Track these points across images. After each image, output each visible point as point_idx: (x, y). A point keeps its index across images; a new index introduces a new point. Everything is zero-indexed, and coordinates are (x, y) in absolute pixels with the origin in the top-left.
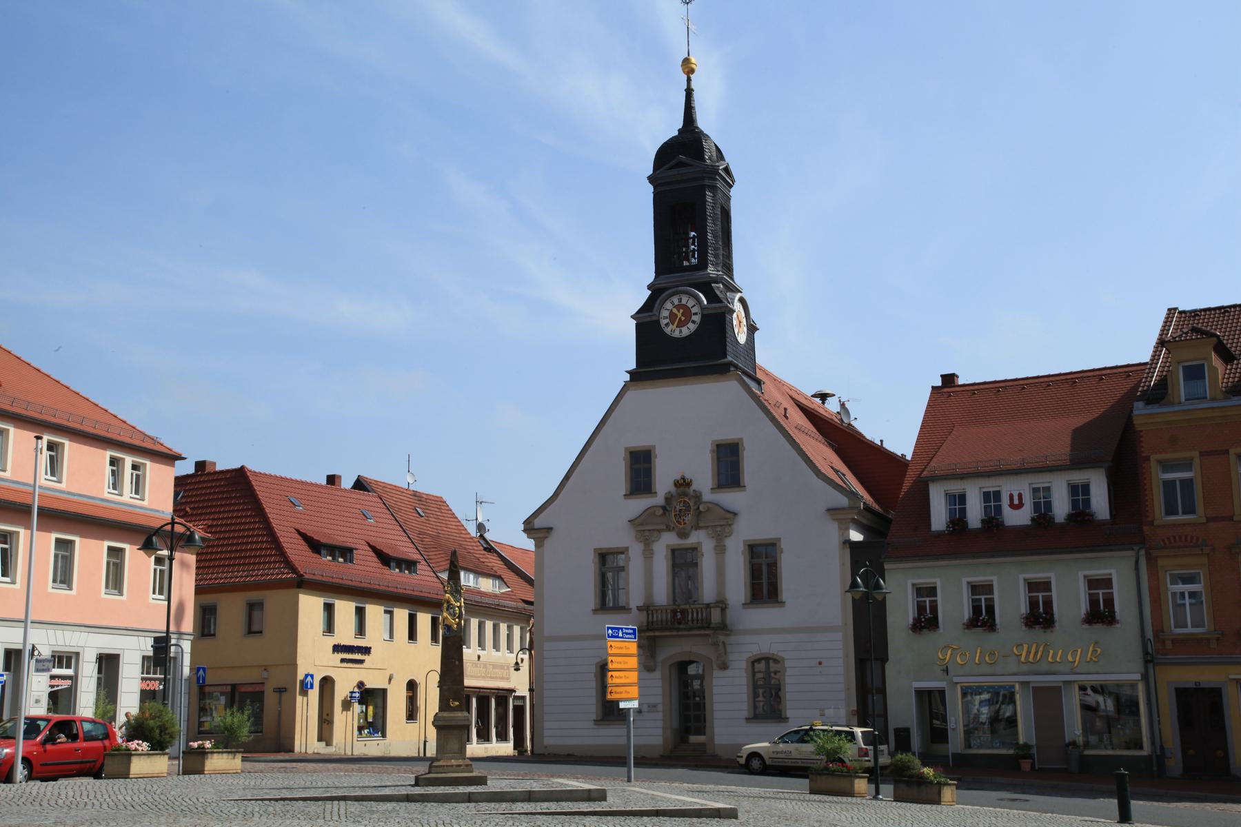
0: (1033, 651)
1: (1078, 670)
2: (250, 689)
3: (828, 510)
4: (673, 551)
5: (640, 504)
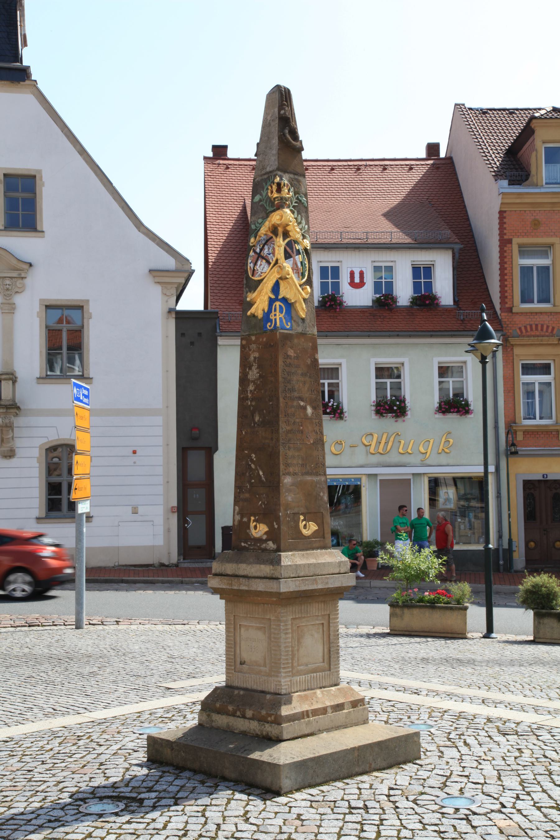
1: (428, 462)
2: (545, 340)
3: (150, 271)
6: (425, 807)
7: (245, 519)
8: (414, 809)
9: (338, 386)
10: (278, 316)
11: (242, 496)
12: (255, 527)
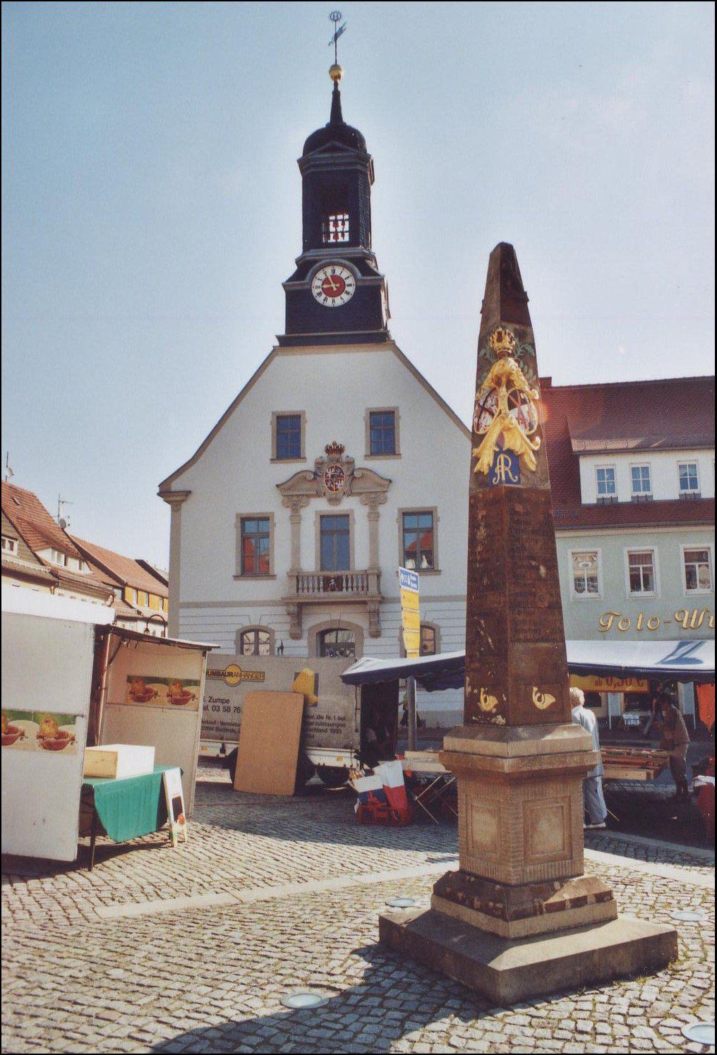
0: (694, 617)
3: (277, 486)
4: (322, 517)
5: (288, 469)
6: (667, 1038)
7: (476, 691)
8: (652, 1040)
9: (652, 570)
10: (502, 470)
11: (472, 666)
12: (485, 700)
